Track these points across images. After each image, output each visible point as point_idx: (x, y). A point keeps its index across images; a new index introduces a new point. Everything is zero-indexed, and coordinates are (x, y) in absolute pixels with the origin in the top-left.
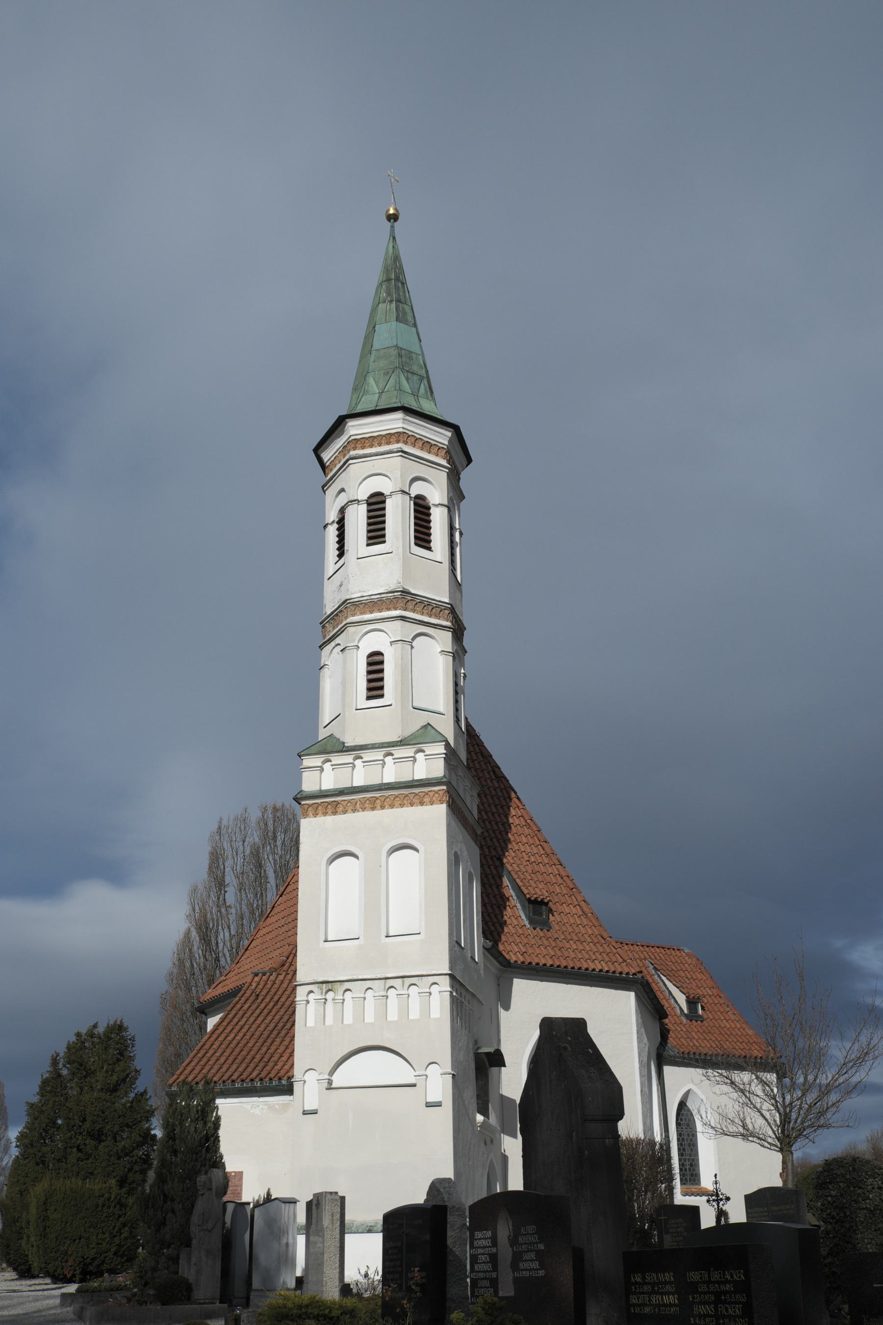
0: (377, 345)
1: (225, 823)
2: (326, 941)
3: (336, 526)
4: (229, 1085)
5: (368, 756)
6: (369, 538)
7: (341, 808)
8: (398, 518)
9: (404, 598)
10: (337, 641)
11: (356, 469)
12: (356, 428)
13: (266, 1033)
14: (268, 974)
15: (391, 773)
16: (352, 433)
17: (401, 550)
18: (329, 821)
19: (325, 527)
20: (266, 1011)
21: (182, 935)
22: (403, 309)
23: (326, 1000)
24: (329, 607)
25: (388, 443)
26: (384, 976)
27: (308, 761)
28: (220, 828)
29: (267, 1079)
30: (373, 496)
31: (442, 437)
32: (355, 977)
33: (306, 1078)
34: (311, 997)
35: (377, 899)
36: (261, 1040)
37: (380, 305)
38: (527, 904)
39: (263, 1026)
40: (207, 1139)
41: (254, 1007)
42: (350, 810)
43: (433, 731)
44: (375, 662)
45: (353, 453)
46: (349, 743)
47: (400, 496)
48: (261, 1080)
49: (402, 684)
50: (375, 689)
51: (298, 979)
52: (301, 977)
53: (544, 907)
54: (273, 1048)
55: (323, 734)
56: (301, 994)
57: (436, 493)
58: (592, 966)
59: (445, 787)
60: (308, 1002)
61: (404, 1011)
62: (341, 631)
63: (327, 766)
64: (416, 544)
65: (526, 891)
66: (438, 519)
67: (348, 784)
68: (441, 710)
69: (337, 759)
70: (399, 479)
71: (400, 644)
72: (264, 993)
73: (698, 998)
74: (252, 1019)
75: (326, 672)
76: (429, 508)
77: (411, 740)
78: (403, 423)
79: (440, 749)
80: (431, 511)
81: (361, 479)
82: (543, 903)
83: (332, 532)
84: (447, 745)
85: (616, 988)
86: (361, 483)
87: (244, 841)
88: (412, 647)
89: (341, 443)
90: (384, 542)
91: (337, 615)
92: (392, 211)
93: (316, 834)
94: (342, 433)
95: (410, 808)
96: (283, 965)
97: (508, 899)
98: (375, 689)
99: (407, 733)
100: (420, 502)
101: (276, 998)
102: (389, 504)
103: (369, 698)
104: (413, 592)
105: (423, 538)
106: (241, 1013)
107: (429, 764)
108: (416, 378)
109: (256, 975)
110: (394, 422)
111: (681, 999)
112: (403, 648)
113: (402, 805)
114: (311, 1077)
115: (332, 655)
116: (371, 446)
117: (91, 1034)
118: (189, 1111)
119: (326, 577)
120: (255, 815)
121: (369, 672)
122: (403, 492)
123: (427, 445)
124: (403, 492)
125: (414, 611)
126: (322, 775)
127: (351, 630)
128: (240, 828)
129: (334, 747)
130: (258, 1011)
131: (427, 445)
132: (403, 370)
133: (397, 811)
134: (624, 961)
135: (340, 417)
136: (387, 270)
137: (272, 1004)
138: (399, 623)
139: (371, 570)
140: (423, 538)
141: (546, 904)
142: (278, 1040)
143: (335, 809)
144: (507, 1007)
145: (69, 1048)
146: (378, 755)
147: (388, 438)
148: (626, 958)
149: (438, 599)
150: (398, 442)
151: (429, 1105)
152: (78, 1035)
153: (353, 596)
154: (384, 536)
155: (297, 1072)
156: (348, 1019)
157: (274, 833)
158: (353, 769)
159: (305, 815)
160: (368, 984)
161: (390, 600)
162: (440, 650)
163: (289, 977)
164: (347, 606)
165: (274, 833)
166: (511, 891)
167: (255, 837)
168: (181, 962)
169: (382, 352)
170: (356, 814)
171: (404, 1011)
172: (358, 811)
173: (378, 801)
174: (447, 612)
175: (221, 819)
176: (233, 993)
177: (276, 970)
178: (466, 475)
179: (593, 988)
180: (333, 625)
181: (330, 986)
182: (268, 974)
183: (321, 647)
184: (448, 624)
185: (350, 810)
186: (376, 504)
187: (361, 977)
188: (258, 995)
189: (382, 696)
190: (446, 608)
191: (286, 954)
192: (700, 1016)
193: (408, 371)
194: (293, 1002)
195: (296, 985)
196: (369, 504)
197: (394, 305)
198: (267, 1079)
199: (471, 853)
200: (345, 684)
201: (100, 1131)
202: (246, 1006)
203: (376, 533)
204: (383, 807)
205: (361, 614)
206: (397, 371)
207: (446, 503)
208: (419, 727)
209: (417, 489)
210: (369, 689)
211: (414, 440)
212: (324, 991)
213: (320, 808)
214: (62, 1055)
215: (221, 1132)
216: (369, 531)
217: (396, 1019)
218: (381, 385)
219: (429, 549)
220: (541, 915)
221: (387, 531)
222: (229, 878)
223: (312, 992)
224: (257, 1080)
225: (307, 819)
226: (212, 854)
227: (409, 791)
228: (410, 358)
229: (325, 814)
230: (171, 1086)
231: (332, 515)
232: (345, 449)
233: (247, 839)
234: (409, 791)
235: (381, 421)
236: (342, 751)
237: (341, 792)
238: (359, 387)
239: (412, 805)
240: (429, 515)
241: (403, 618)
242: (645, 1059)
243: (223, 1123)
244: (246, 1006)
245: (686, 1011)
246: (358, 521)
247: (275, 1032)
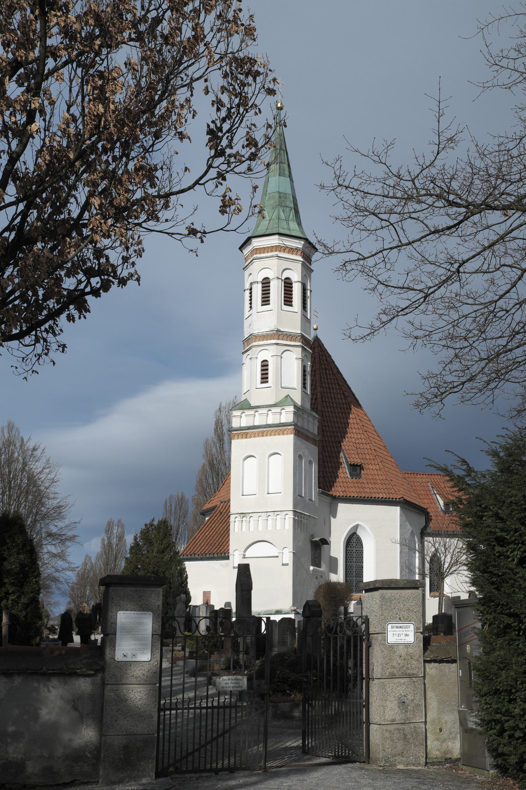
0: (269, 191)
3: (249, 291)
4: (204, 556)
5: (261, 411)
6: (263, 301)
7: (249, 435)
9: (278, 334)
10: (249, 353)
11: (257, 265)
12: (257, 243)
18: (244, 441)
25: (272, 251)
28: (220, 409)
31: (299, 244)
34: (237, 519)
35: (265, 478)
40: (183, 583)
44: (265, 365)
46: (253, 404)
50: (264, 378)
56: (232, 518)
57: (296, 276)
58: (377, 496)
64: (285, 304)
68: (295, 387)
69: (248, 412)
71: (275, 357)
75: (244, 366)
76: (292, 284)
79: (291, 409)
80: (293, 285)
82: (357, 465)
83: (247, 293)
84: (295, 406)
88: (281, 357)
92: (279, 105)
93: (238, 448)
94: (250, 244)
97: (341, 463)
98: (264, 378)
99: (278, 400)
100: (287, 281)
102: (272, 284)
103: (262, 383)
105: (288, 301)
107: (287, 415)
108: (288, 209)
110: (274, 241)
111: (442, 502)
113: (275, 435)
114: (236, 553)
116: (264, 253)
117: (151, 525)
121: (262, 370)
123: (292, 250)
125: (282, 339)
126: (241, 419)
127: (254, 349)
129: (245, 406)
131: (292, 250)
132: (281, 206)
133: (273, 437)
138: (275, 347)
140: (288, 301)
143: (246, 436)
144: (335, 517)
145: (142, 532)
146: (265, 411)
150: (276, 251)
151: (283, 565)
152: (146, 525)
155: (231, 551)
160: (260, 514)
161: (271, 335)
164: (252, 337)
176: (213, 508)
183: (243, 353)
184: (300, 344)
186: (266, 283)
189: (267, 382)
196: (263, 284)
199: (312, 452)
201: (157, 571)
203: (266, 301)
204: (267, 435)
207: (300, 280)
209: (286, 274)
210: (262, 378)
214: (139, 535)
215: (188, 580)
218: (270, 216)
219: (291, 305)
220: (356, 471)
221: (271, 299)
227: (278, 428)
228: (286, 198)
229: (242, 438)
231: (247, 286)
234: (278, 428)
237: (249, 428)
240: (292, 287)
242: (408, 536)
243: (189, 576)
246: (258, 290)
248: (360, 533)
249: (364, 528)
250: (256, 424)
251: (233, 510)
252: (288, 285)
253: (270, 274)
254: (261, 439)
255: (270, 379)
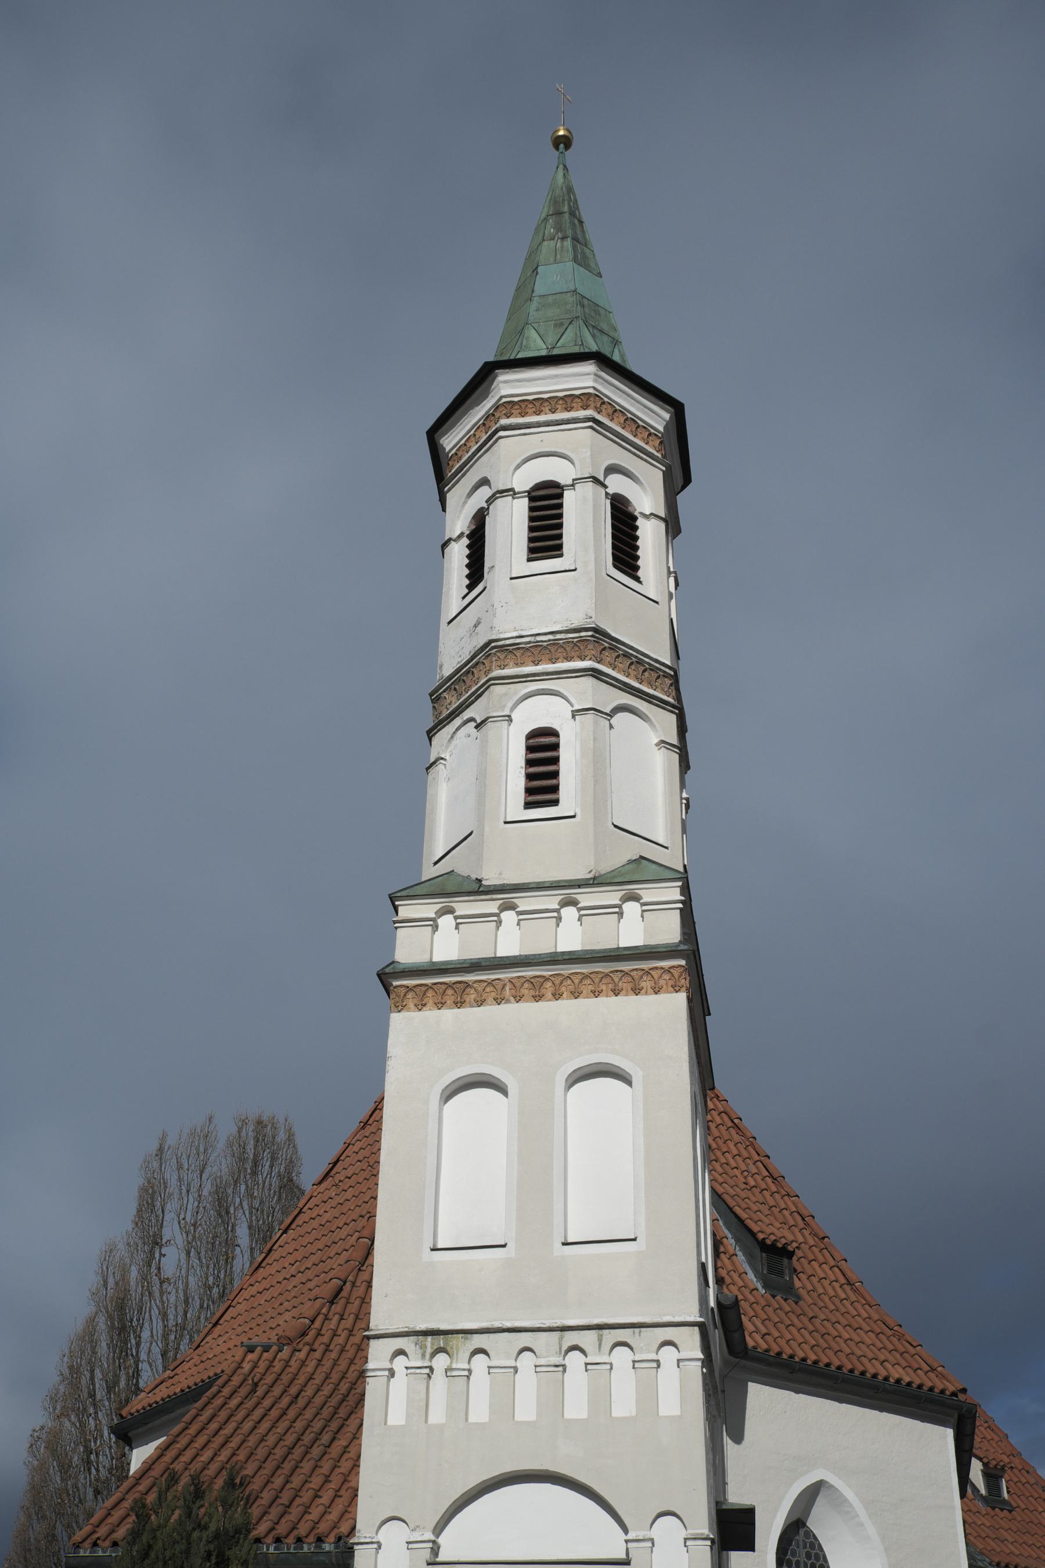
0: (540, 288)
1: (171, 1141)
2: (434, 1249)
3: (465, 541)
5: (526, 902)
7: (472, 996)
8: (584, 522)
9: (596, 643)
10: (467, 714)
11: (510, 447)
12: (509, 385)
13: (279, 1452)
14: (275, 1348)
15: (571, 935)
16: (504, 392)
17: (592, 567)
19: (445, 545)
20: (274, 1413)
21: (80, 1325)
22: (583, 252)
23: (431, 1369)
24: (449, 661)
25: (568, 409)
26: (559, 1323)
27: (407, 910)
28: (161, 1149)
29: (291, 1540)
30: (539, 486)
31: (658, 418)
32: (497, 1324)
33: (381, 1537)
34: (400, 1362)
36: (270, 1466)
37: (545, 243)
38: (757, 1251)
39: (271, 1439)
41: (249, 1404)
42: (490, 1000)
43: (654, 866)
44: (543, 749)
45: (504, 422)
46: (491, 878)
47: (590, 485)
48: (278, 1540)
49: (596, 782)
51: (371, 1325)
52: (380, 1318)
53: (786, 1261)
54: (296, 1481)
55: (429, 872)
56: (378, 1354)
57: (646, 498)
58: (896, 1373)
59: (683, 962)
60: (392, 1373)
61: (600, 1399)
62: (478, 696)
63: (446, 922)
64: (615, 566)
65: (755, 1228)
66: (650, 536)
67: (488, 954)
69: (464, 907)
70: (589, 460)
71: (590, 716)
72: (269, 1379)
73: (1003, 1468)
74: (248, 1425)
75: (441, 771)
76: (635, 518)
77: (614, 877)
78: (595, 381)
80: (638, 523)
81: (518, 462)
83: (458, 554)
85: (924, 1419)
86: (518, 467)
87: (202, 1173)
89: (482, 413)
90: (561, 556)
91: (468, 672)
92: (561, 133)
93: (419, 1044)
94: (485, 395)
95: (614, 999)
96: (304, 1334)
101: (293, 1390)
103: (528, 805)
104: (613, 634)
105: (625, 555)
106: (223, 1415)
109: (251, 1350)
110: (582, 377)
112: (596, 723)
113: (596, 993)
114: (393, 1536)
115: (454, 742)
116: (538, 412)
118: (187, 1552)
119: (444, 620)
120: (225, 1130)
122: (596, 480)
124: (596, 480)
127: (497, 690)
128: (197, 1149)
129: (454, 888)
130: (258, 1413)
134: (933, 1370)
135: (486, 364)
136: (555, 202)
137: (286, 1400)
138: (588, 682)
139: (534, 598)
140: (625, 555)
141: (790, 1255)
142: (307, 1466)
143: (460, 997)
144: (738, 1438)
147: (569, 401)
148: (935, 1365)
149: (655, 656)
150: (585, 407)
153: (502, 636)
154: (560, 547)
156: (479, 1412)
157: (255, 1163)
158: (498, 928)
159: (400, 1007)
162: (656, 741)
163: (348, 1323)
164: (492, 651)
165: (255, 1163)
166: (726, 1232)
167: (221, 1165)
168: (74, 1370)
169: (550, 299)
170: (504, 1007)
171: (600, 1399)
172: (508, 1001)
173: (549, 984)
174: (668, 682)
175: (164, 1138)
177: (290, 1341)
178: (683, 499)
179: (885, 1415)
180: (455, 697)
181: (441, 1341)
182: (275, 1348)
183: (430, 734)
185: (490, 1000)
186: (546, 506)
187: (508, 1324)
188: (256, 1385)
189: (555, 802)
190: (666, 675)
191: (311, 1313)
192: (1005, 1502)
193: (594, 327)
194: (362, 1375)
195: (368, 1338)
196: (532, 499)
197: (568, 243)
198: (291, 1540)
200: (484, 782)
202: (234, 1403)
203: (545, 538)
205: (517, 665)
206: (576, 324)
208: (624, 860)
209: (617, 484)
211: (616, 411)
212: (429, 1351)
213: (430, 993)
216: (531, 540)
217: (584, 1415)
219: (637, 579)
220: (781, 1274)
222: (171, 1231)
223: (401, 1352)
224: (269, 1540)
225: (403, 1014)
226: (143, 1190)
227: (611, 969)
229: (440, 1005)
230: (77, 1546)
231: (459, 522)
232: (489, 416)
233: (208, 1169)
234: (611, 969)
235: (556, 376)
236: (478, 893)
238: (516, 329)
239: (616, 992)
241: (596, 674)
244: (234, 1403)
245: (983, 1491)
246: (511, 524)
247: (298, 1452)
248: (823, 1525)
249: (839, 1502)
250: (439, 957)
251: (383, 1314)
252: (623, 521)
253: (558, 471)
254: (528, 1009)
255: (564, 793)
